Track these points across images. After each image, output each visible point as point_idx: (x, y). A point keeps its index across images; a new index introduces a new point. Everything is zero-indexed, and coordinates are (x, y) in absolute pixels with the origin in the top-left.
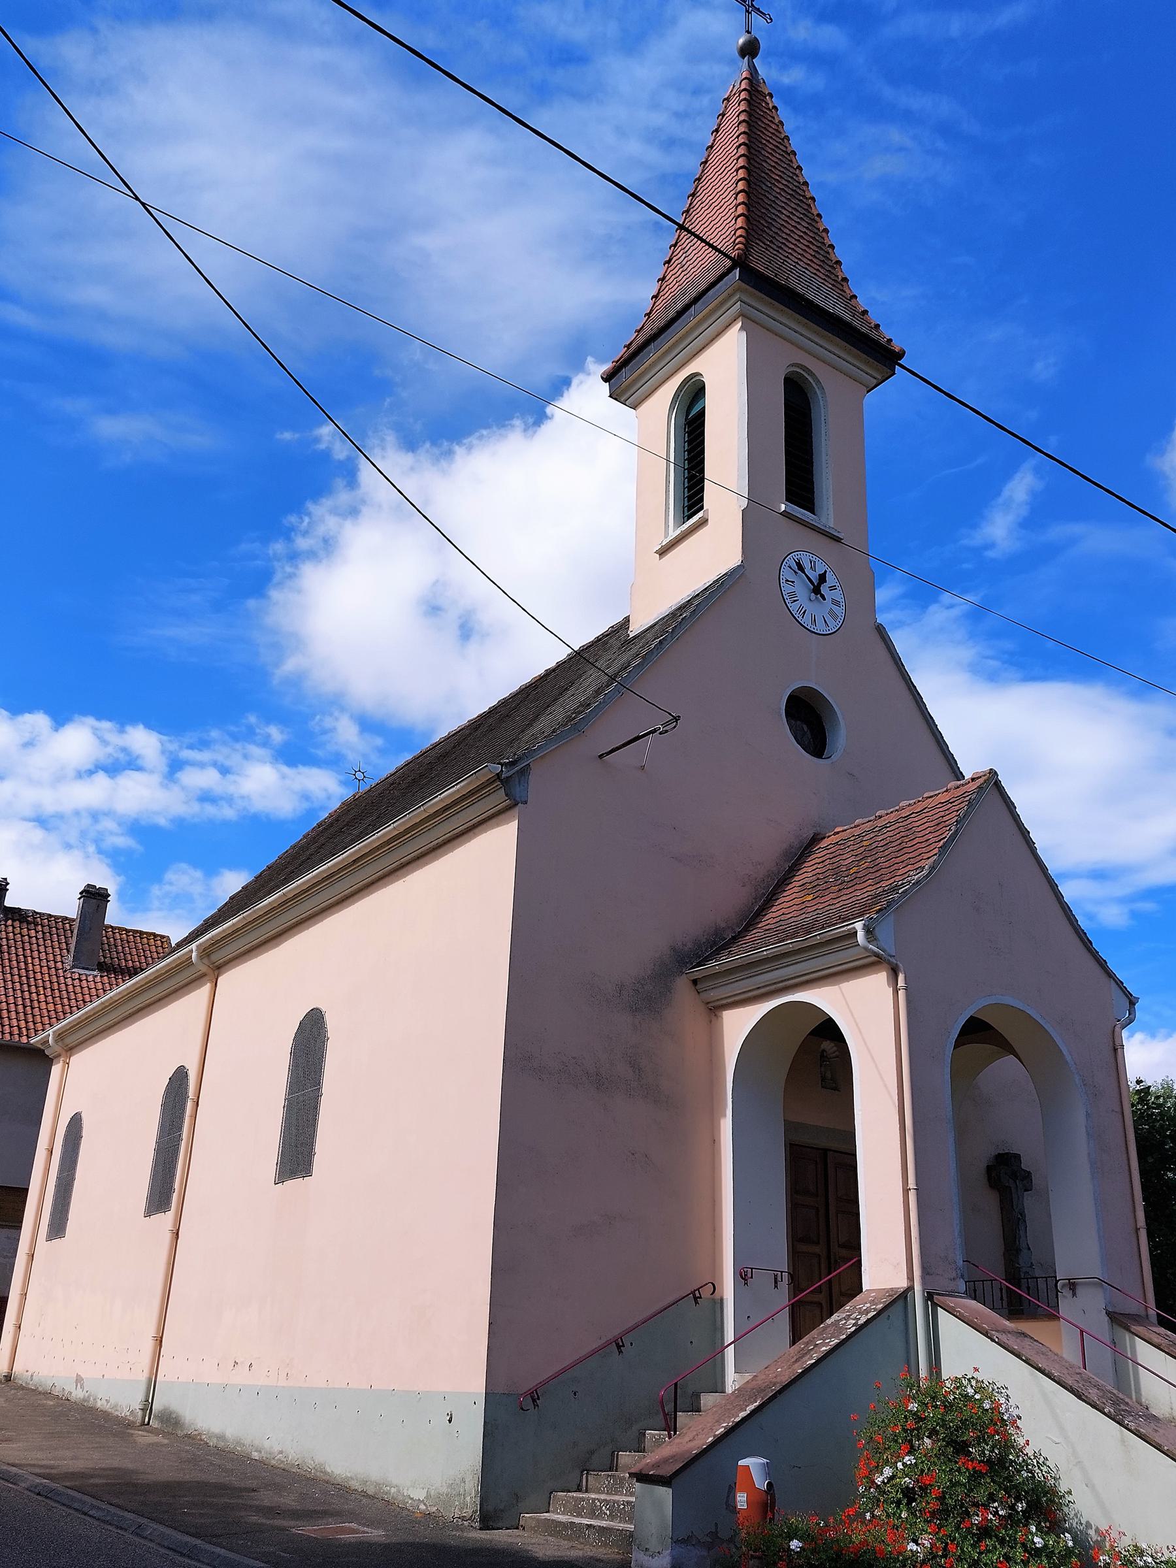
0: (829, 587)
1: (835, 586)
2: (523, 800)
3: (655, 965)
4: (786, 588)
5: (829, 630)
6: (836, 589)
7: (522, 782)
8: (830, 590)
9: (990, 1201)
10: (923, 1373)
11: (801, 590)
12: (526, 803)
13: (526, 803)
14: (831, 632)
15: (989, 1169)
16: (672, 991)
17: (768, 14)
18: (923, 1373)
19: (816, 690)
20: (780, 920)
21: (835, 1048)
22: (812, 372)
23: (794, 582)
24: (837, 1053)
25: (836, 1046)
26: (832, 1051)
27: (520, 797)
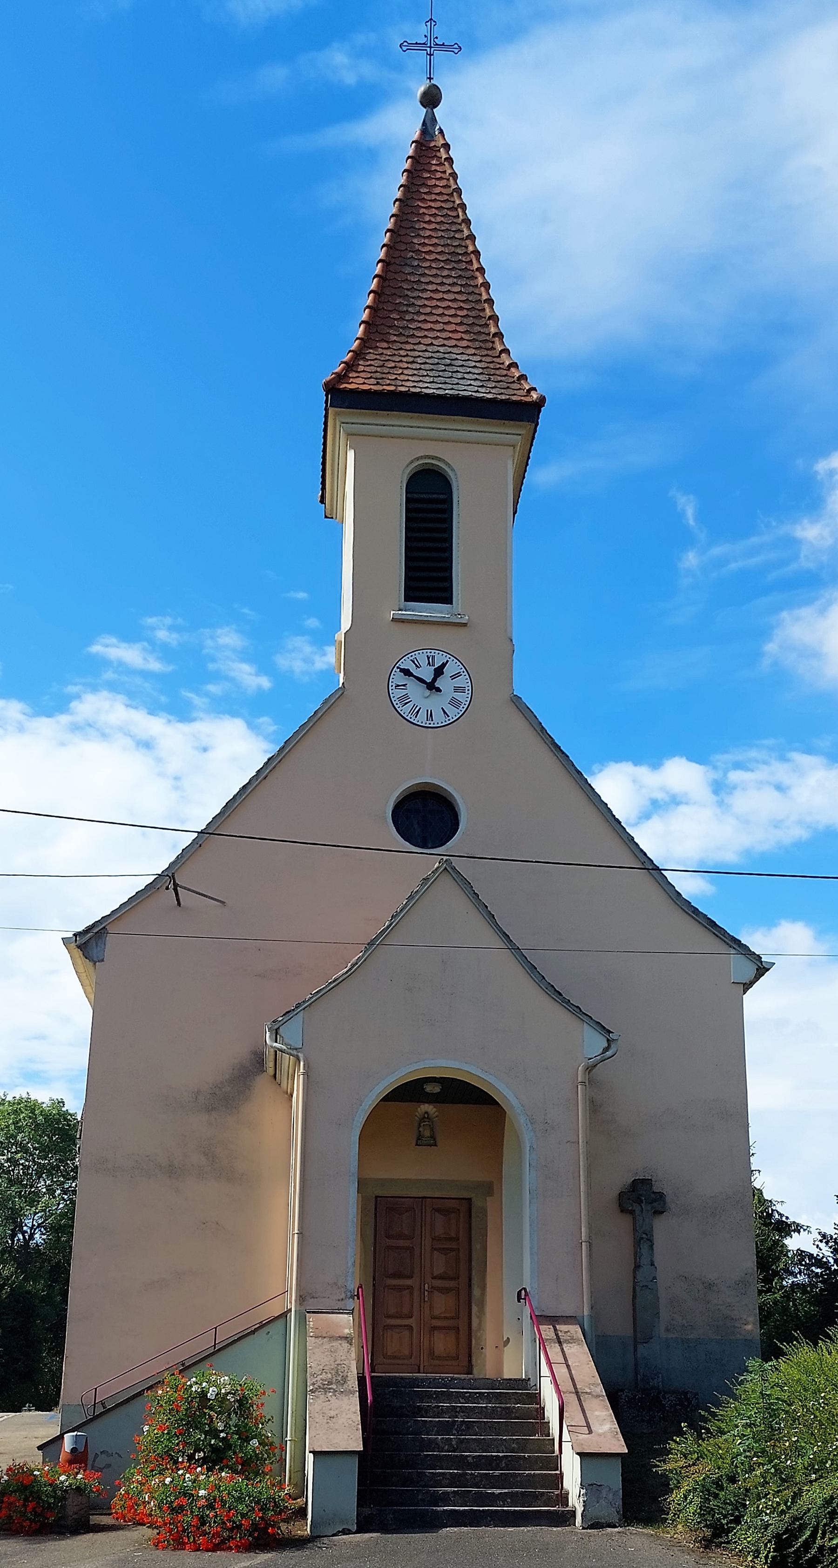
0: (451, 677)
1: (460, 672)
2: (101, 958)
3: (233, 1069)
4: (397, 694)
5: (465, 704)
6: (461, 675)
7: (99, 944)
8: (452, 679)
9: (621, 1226)
10: (329, 396)
11: (415, 691)
12: (103, 960)
13: (103, 960)
14: (466, 707)
15: (621, 1195)
16: (251, 1088)
17: (405, 42)
18: (329, 396)
19: (439, 786)
20: (445, 390)
21: (434, 1110)
22: (440, 458)
23: (406, 684)
24: (437, 1113)
25: (435, 1107)
26: (432, 1112)
27: (98, 957)
